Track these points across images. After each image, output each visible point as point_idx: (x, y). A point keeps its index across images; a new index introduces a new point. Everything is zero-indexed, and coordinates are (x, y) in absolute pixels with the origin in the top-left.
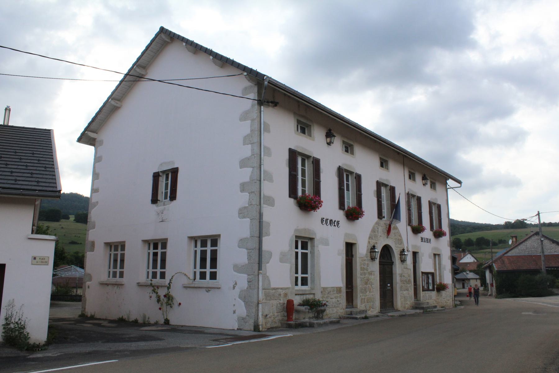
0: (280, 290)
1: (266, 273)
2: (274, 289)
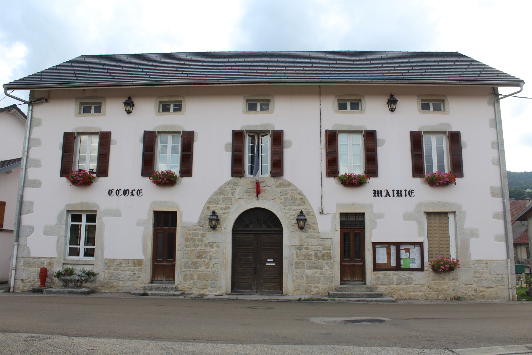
0: (43, 259)
1: (27, 245)
2: (35, 258)
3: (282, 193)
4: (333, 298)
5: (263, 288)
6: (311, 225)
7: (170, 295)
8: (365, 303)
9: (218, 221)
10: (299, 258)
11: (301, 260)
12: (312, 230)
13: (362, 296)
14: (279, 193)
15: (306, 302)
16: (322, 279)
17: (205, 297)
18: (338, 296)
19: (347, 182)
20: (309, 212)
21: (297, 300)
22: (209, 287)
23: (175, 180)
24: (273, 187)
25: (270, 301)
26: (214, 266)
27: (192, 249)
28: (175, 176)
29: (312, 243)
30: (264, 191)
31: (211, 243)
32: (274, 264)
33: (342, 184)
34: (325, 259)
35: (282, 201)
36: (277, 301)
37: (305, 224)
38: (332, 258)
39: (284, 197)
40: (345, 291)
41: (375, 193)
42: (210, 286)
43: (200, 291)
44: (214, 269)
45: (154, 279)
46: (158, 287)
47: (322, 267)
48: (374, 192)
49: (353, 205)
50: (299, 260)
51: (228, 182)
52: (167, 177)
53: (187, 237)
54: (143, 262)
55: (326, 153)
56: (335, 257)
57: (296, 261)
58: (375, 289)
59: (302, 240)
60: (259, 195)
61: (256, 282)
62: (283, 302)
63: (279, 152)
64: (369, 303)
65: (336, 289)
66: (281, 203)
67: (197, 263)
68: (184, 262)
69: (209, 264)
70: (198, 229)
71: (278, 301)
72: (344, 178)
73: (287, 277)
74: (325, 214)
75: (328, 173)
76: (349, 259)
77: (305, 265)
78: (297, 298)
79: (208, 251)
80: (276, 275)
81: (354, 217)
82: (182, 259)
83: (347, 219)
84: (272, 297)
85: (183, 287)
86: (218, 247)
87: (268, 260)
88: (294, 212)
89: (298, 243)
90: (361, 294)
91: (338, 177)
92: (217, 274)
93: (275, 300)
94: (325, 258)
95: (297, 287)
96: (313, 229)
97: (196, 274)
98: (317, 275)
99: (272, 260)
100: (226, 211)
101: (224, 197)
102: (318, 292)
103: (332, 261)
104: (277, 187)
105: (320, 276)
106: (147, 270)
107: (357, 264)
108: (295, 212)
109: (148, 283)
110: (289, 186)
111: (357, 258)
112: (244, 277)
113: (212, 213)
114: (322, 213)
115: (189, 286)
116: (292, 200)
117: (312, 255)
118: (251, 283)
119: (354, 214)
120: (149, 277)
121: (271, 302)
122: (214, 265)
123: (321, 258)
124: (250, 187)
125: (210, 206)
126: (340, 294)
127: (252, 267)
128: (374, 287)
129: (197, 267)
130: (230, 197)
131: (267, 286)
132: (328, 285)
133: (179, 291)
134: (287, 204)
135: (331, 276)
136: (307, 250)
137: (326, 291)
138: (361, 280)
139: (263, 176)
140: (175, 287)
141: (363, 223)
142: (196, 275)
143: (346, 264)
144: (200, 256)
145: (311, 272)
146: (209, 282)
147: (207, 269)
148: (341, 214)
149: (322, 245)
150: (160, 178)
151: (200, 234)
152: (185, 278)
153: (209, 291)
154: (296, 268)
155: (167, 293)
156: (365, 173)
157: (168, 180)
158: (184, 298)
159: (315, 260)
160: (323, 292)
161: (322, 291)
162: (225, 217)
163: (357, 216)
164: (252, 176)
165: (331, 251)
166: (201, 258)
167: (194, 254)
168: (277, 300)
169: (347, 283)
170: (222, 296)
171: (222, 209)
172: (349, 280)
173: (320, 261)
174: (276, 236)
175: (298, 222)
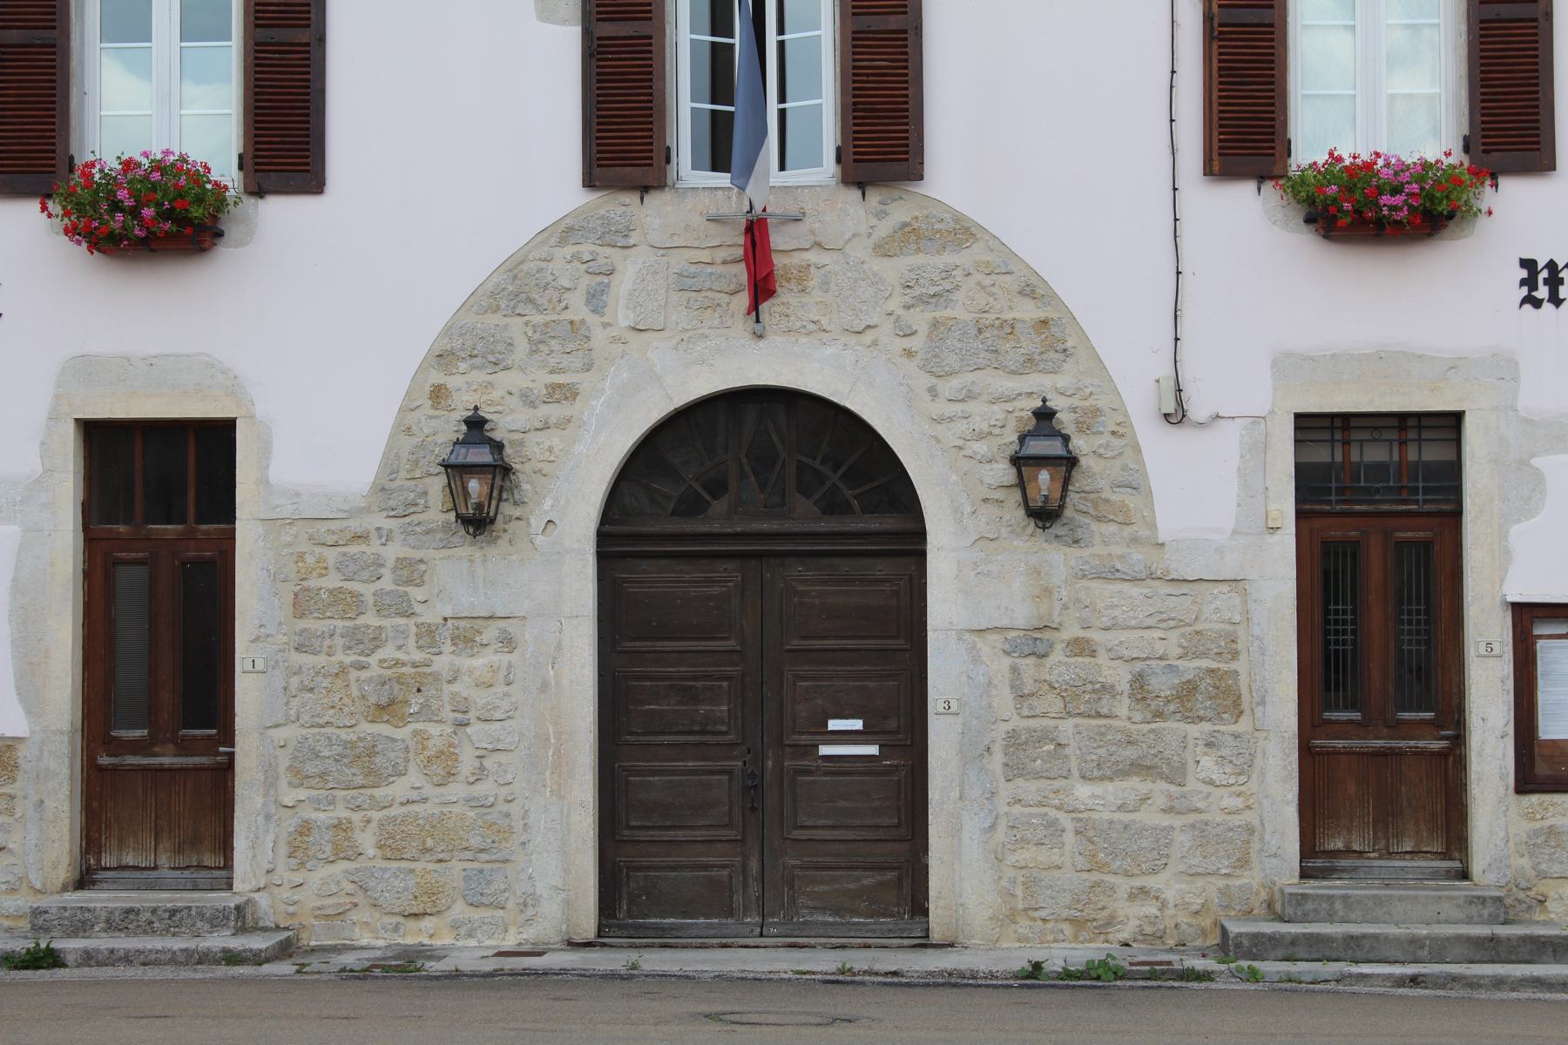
3: (917, 291)
4: (1245, 964)
5: (802, 900)
6: (1104, 495)
7: (204, 958)
8: (1453, 994)
9: (503, 479)
10: (1031, 708)
11: (1045, 722)
12: (1112, 528)
13: (1439, 949)
14: (899, 290)
15: (1074, 987)
16: (1183, 839)
17: (428, 964)
18: (1280, 953)
19: (1340, 210)
20: (1096, 412)
21: (1016, 977)
22: (454, 902)
23: (215, 218)
24: (860, 251)
25: (842, 981)
26: (482, 768)
27: (341, 663)
28: (209, 186)
29: (1117, 612)
30: (800, 280)
31: (462, 623)
32: (873, 750)
33: (1312, 227)
34: (1202, 713)
35: (916, 343)
36: (889, 980)
37: (1065, 489)
38: (1245, 706)
39: (929, 316)
40: (1331, 918)
41: (1530, 282)
42: (464, 897)
43: (396, 929)
44: (484, 789)
45: (99, 861)
46: (129, 911)
47: (1184, 765)
48: (1524, 274)
49: (1383, 361)
50: (1032, 723)
51: (562, 227)
52: (159, 196)
53: (305, 583)
54: (22, 752)
55: (1208, 18)
56: (1262, 702)
57: (1009, 726)
58: (1530, 907)
59: (1047, 592)
60: (764, 307)
61: (754, 865)
62: (927, 985)
63: (893, 22)
64: (1482, 995)
65: (1270, 905)
66: (909, 353)
67: (371, 752)
68: (290, 749)
69: (455, 757)
70: (374, 535)
71: (896, 980)
72: (1320, 189)
73: (956, 831)
74: (1200, 425)
75: (1215, 156)
76: (1356, 716)
77: (1067, 751)
78: (1019, 961)
79: (446, 675)
80: (887, 822)
81: (1391, 441)
82: (277, 726)
83: (1346, 455)
84: (859, 960)
85: (291, 909)
86: (508, 643)
87: (834, 725)
88: (998, 411)
89: (1022, 615)
90: (1428, 937)
91: (1284, 176)
92: (508, 815)
93: (877, 974)
94: (1202, 705)
95: (1019, 892)
96: (1120, 518)
97: (368, 821)
98: (1149, 817)
99: (857, 724)
100: (554, 412)
101: (538, 319)
102: (1154, 924)
103: (1244, 725)
104: (883, 250)
105: (1166, 820)
106: (49, 803)
107: (1412, 743)
108: (1001, 416)
109: (59, 884)
110: (959, 246)
111: (1410, 710)
112: (680, 835)
113: (464, 428)
114: (1177, 417)
115: (329, 901)
116: (980, 331)
117: (1112, 687)
118: (725, 872)
119: (1395, 422)
120: (67, 845)
121: (850, 988)
122: (487, 763)
123: (1172, 707)
124: (705, 256)
125: (453, 382)
126: (1295, 940)
127: (729, 772)
128: (1522, 895)
129: (375, 777)
130: (576, 318)
131: (827, 888)
132: (1221, 883)
133: (265, 929)
134: (952, 360)
135: (1236, 820)
136: (1080, 659)
137: (1207, 922)
138: (1437, 847)
139: (791, 177)
140: (238, 908)
141: (1449, 479)
142: (374, 824)
143: (1340, 744)
144: (392, 703)
145: (1111, 798)
146: (456, 867)
147: (440, 790)
148: (1307, 425)
149: (1181, 624)
150: (116, 206)
151: (390, 563)
152: (300, 846)
153: (455, 926)
154: (1015, 770)
155: (184, 945)
156: (1466, 149)
157: (167, 215)
158: (298, 972)
159: (1137, 717)
160: (1184, 927)
161: (1183, 918)
162: (550, 450)
163: (1412, 435)
164: (723, 179)
165: (1240, 665)
166: (402, 720)
167: (355, 693)
168: (886, 974)
169: (1344, 870)
170: (540, 954)
171: (528, 399)
172: (1356, 847)
173: (1170, 724)
174: (882, 568)
175: (1020, 475)
